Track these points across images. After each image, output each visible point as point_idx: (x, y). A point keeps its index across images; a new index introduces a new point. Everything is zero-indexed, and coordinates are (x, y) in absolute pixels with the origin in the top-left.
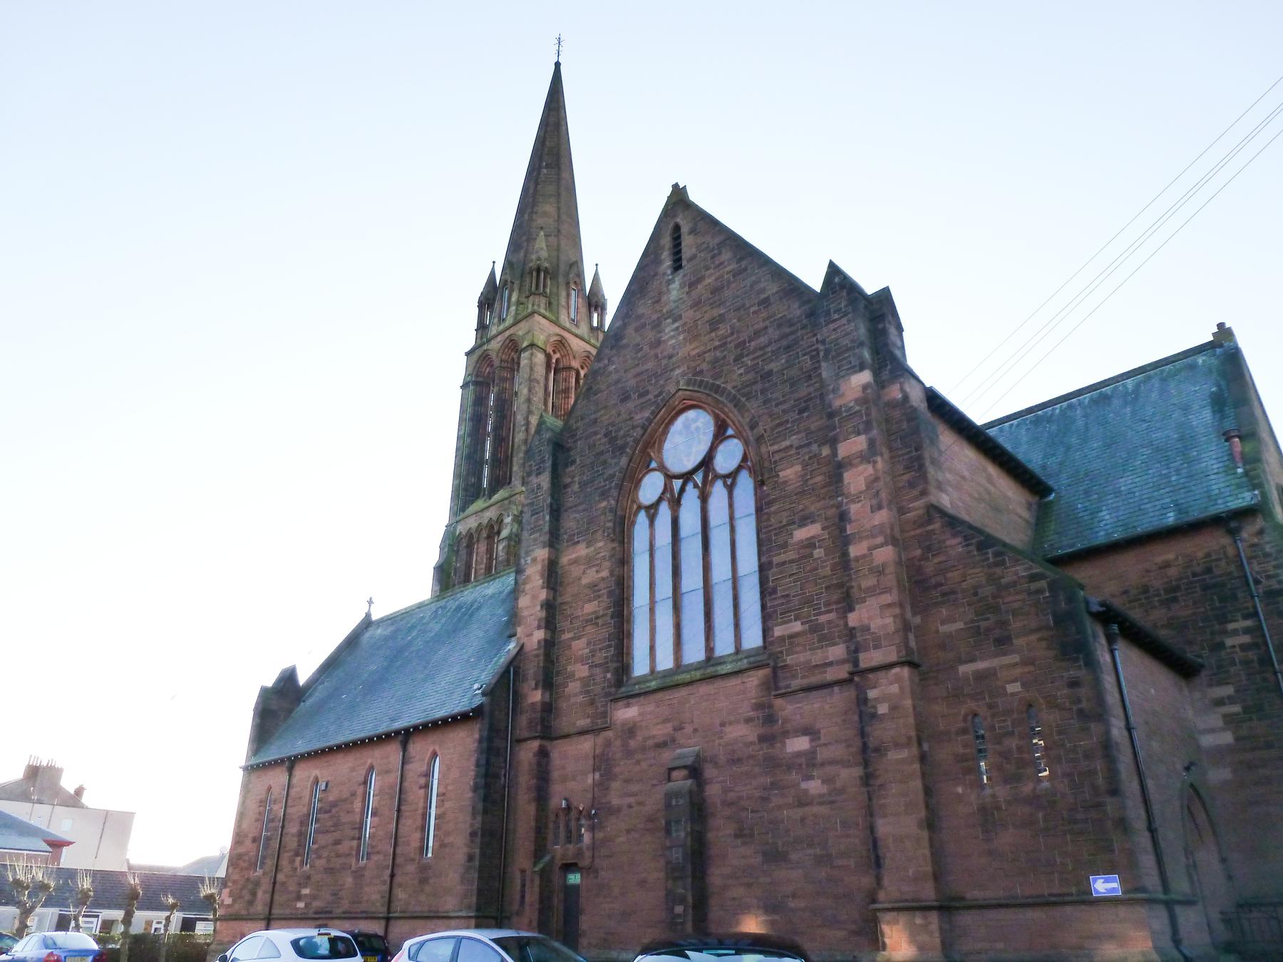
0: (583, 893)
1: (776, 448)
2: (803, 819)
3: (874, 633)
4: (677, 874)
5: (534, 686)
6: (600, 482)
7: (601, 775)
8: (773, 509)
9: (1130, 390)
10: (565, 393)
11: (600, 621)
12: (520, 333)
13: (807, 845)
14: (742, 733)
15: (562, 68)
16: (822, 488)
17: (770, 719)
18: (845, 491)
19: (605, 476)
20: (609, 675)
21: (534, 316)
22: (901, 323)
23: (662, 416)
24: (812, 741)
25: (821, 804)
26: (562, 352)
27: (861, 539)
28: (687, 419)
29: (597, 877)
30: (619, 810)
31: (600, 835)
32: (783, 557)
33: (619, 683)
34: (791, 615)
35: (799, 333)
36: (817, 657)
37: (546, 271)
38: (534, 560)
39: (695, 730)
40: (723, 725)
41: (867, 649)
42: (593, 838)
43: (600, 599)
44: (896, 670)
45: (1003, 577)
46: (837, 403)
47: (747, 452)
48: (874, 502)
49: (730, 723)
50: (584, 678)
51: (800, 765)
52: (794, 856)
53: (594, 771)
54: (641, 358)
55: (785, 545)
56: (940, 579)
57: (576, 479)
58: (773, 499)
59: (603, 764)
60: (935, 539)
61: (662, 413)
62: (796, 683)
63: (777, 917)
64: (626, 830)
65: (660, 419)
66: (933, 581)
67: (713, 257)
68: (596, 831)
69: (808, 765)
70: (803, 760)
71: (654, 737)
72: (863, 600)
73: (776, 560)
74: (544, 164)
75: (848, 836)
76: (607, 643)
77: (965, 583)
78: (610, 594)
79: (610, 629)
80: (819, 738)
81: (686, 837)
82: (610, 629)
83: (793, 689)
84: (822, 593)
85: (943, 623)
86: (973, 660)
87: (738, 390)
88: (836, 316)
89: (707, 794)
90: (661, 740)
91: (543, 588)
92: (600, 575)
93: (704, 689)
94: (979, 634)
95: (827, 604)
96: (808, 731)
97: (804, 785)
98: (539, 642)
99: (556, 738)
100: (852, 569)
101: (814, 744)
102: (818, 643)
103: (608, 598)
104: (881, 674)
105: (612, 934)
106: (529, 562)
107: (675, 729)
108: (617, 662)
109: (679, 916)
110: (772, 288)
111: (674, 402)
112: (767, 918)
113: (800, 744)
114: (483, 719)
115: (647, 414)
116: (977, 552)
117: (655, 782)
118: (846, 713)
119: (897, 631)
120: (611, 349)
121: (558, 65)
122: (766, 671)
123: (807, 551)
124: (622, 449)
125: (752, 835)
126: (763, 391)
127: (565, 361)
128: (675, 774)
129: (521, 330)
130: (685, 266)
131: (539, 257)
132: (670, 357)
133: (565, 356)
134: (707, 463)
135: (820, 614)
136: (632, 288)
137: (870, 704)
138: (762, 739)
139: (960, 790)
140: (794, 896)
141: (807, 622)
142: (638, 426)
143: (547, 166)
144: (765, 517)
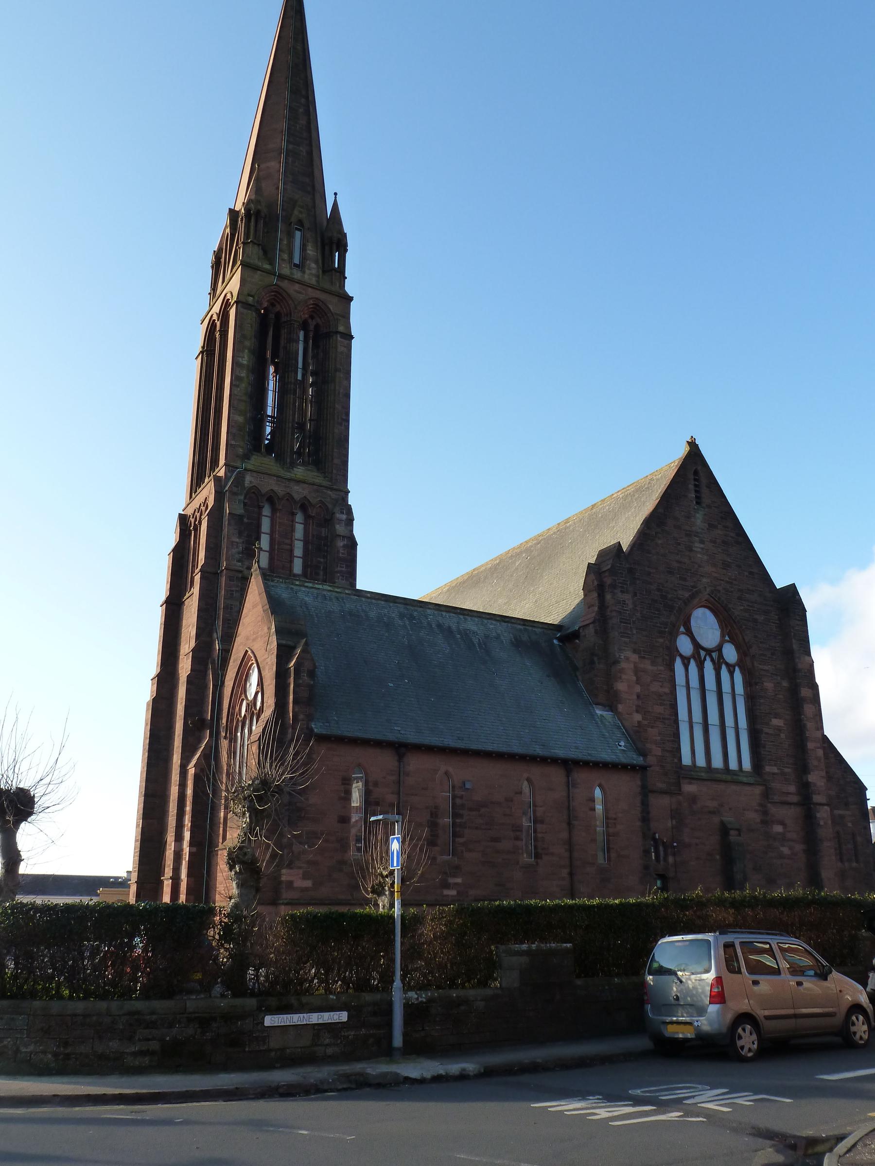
9: (33, 1044)
14: (753, 816)
17: (765, 813)
22: (821, 709)
40: (744, 810)
47: (697, 607)
50: (659, 756)
59: (676, 814)
60: (857, 1019)
76: (672, 739)
96: (782, 823)
113: (778, 829)
120: (706, 590)
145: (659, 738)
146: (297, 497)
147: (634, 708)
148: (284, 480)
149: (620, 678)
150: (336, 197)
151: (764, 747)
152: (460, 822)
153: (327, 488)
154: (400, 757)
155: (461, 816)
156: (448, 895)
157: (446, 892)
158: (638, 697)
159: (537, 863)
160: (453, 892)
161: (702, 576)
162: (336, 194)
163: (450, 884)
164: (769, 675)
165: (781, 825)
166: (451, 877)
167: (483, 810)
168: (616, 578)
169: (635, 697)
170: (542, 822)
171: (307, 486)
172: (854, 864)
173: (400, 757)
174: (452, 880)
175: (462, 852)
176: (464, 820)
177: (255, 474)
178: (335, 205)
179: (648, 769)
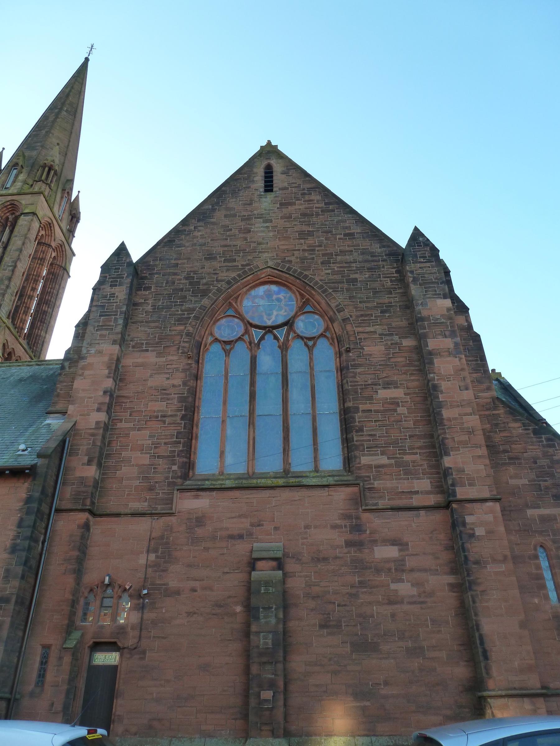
0: (121, 676)
1: (360, 329)
2: (393, 615)
3: (468, 474)
4: (265, 659)
5: (86, 461)
6: (178, 311)
7: (157, 557)
8: (358, 370)
10: (41, 261)
11: (167, 420)
12: (23, 202)
13: (399, 638)
15: (89, 63)
16: (403, 366)
17: (357, 528)
18: (436, 371)
19: (183, 308)
20: (175, 468)
21: (40, 196)
23: (248, 281)
24: (400, 550)
25: (410, 603)
26: (47, 232)
27: (452, 407)
28: (269, 291)
29: (143, 659)
30: (178, 592)
31: (149, 615)
32: (367, 407)
33: (185, 477)
34: (378, 450)
35: (381, 263)
36: (404, 485)
37: (56, 173)
38: (100, 352)
39: (276, 529)
40: (307, 527)
41: (463, 485)
42: (142, 618)
43: (169, 402)
44: (490, 504)
45: (555, 456)
46: (425, 313)
48: (462, 384)
49: (316, 527)
50: (144, 465)
51: (390, 570)
52: (385, 648)
53: (148, 552)
54: (229, 236)
55: (371, 398)
56: (507, 447)
57: (150, 302)
58: (358, 364)
60: (501, 421)
61: (249, 278)
62: (382, 504)
63: (368, 704)
64: (186, 613)
65: (246, 282)
66: (501, 448)
67: (303, 194)
68: (145, 611)
69: (396, 570)
70: (392, 565)
71: (227, 529)
72: (458, 449)
73: (362, 407)
74: (65, 109)
75: (439, 632)
77: (526, 454)
78: (182, 399)
79: (179, 428)
80: (408, 549)
81: (277, 623)
82: (179, 428)
83: (380, 507)
84: (406, 439)
85: (511, 478)
86: (539, 507)
87: (326, 283)
88: (422, 260)
89: (288, 586)
90: (236, 532)
91: (108, 377)
92: (171, 382)
93: (286, 494)
94: (541, 490)
95: (411, 448)
97: (393, 586)
98: (97, 423)
99: (101, 516)
100: (445, 425)
101: (401, 554)
102: (404, 475)
103: (179, 402)
104: (477, 505)
105: (160, 720)
106: (93, 352)
107: (252, 525)
108: (186, 458)
109: (266, 701)
110: (357, 229)
111: (261, 274)
112: (358, 704)
114: (34, 479)
115: (234, 275)
116: (534, 435)
117: (226, 570)
118: (432, 532)
119: (488, 476)
121: (87, 60)
122: (355, 489)
123: (392, 407)
124: (205, 293)
125: (339, 626)
126: (348, 290)
127: (47, 239)
128: (260, 564)
129: (24, 200)
130: (276, 191)
131: (54, 160)
132: (259, 244)
133: (49, 236)
134: (289, 324)
135: (405, 454)
136: (223, 188)
137: (468, 527)
138: (349, 544)
139: (536, 601)
140: (386, 683)
141: (393, 458)
142: (222, 281)
143: (67, 111)
144: (352, 375)
145: (150, 442)
147: (96, 406)
150: (79, 193)
151: (361, 430)
161: (261, 252)
162: (79, 192)
164: (378, 336)
165: (393, 545)
172: (273, 609)
178: (77, 197)
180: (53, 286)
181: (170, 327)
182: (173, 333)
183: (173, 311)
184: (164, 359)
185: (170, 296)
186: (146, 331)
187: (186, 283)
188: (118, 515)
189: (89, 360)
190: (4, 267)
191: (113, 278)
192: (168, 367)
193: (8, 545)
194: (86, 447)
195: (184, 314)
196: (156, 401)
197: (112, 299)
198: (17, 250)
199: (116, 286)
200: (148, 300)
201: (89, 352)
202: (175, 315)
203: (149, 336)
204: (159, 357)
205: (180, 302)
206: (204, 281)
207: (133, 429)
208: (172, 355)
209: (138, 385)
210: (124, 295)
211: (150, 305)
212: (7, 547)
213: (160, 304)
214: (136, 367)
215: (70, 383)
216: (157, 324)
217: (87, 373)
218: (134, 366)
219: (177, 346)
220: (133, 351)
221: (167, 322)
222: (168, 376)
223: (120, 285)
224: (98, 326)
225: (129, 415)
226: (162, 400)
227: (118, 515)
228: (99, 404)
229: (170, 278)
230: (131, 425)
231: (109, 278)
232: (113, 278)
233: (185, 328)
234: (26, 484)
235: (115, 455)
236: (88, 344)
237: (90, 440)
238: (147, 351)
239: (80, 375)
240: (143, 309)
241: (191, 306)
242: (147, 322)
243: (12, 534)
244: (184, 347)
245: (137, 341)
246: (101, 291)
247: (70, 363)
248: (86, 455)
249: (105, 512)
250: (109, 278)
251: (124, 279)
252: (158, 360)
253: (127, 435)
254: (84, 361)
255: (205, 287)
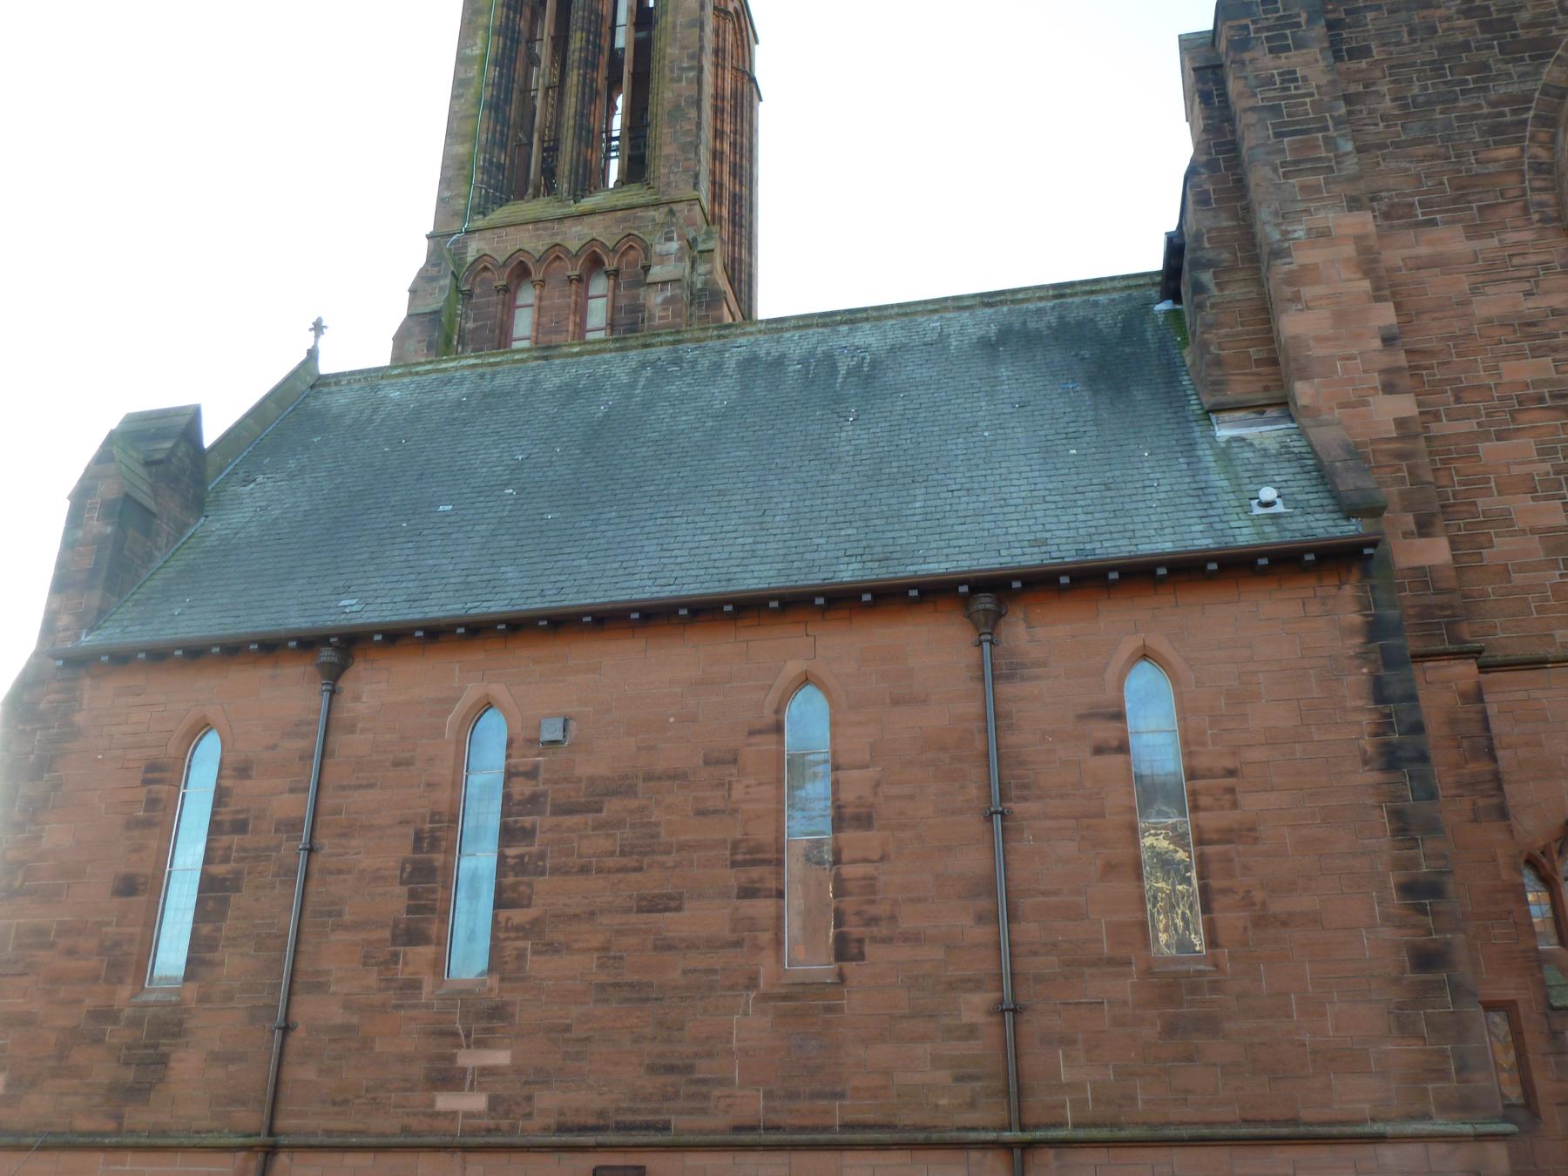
6: (1478, 106)
19: (1493, 96)
43: (1558, 356)
57: (1383, 87)
146: (574, 246)
147: (1376, 379)
148: (549, 224)
149: (1296, 298)
152: (521, 857)
153: (646, 206)
154: (333, 675)
155: (528, 834)
156: (453, 1114)
157: (445, 1101)
158: (1388, 340)
159: (842, 978)
160: (476, 1102)
163: (464, 1070)
166: (468, 1047)
167: (613, 807)
168: (1247, 21)
169: (1377, 343)
170: (864, 820)
171: (601, 217)
173: (333, 675)
174: (469, 1059)
175: (521, 956)
176: (535, 849)
177: (488, 234)
179: (1367, 551)
180: (738, 127)
181: (1475, 153)
182: (1492, 168)
183: (1464, 107)
184: (1495, 242)
185: (1437, 67)
186: (1406, 170)
187: (1471, 27)
188: (1537, 664)
189: (1302, 257)
190: (672, 71)
191: (1268, 29)
192: (1516, 261)
193: (1369, 749)
194: (1395, 489)
195: (1503, 115)
196: (1519, 355)
197: (1292, 86)
198: (691, 24)
199: (1287, 49)
200: (1374, 84)
201: (1291, 236)
202: (1475, 117)
203: (1421, 182)
204: (1479, 237)
205: (1475, 81)
206: (1525, 16)
207: (1483, 436)
208: (1515, 229)
209: (1445, 318)
210: (1323, 72)
211: (1388, 98)
212: (1369, 754)
213: (1416, 91)
214: (1419, 269)
215: (1240, 328)
216: (1430, 148)
217: (1308, 292)
218: (1411, 269)
219: (1520, 204)
220: (1392, 227)
221: (1460, 139)
222: (1526, 286)
223: (1298, 47)
224: (1283, 164)
225: (1452, 399)
226: (1536, 352)
227: (1537, 664)
228: (1383, 371)
229: (1416, 17)
230: (1470, 426)
231: (1257, 31)
232: (1268, 29)
233: (1523, 149)
234: (1347, 587)
235: (1455, 509)
236: (1276, 214)
237: (1400, 470)
238: (1432, 223)
239: (1291, 300)
240: (1371, 112)
241: (1514, 89)
242: (1396, 145)
243: (1367, 720)
244: (1541, 204)
245: (1390, 198)
246: (1249, 68)
247: (1214, 273)
248: (1406, 509)
249: (1489, 659)
250: (1257, 31)
251: (1304, 27)
252: (1477, 245)
253: (1472, 454)
254: (1284, 261)
255: (1535, 33)
